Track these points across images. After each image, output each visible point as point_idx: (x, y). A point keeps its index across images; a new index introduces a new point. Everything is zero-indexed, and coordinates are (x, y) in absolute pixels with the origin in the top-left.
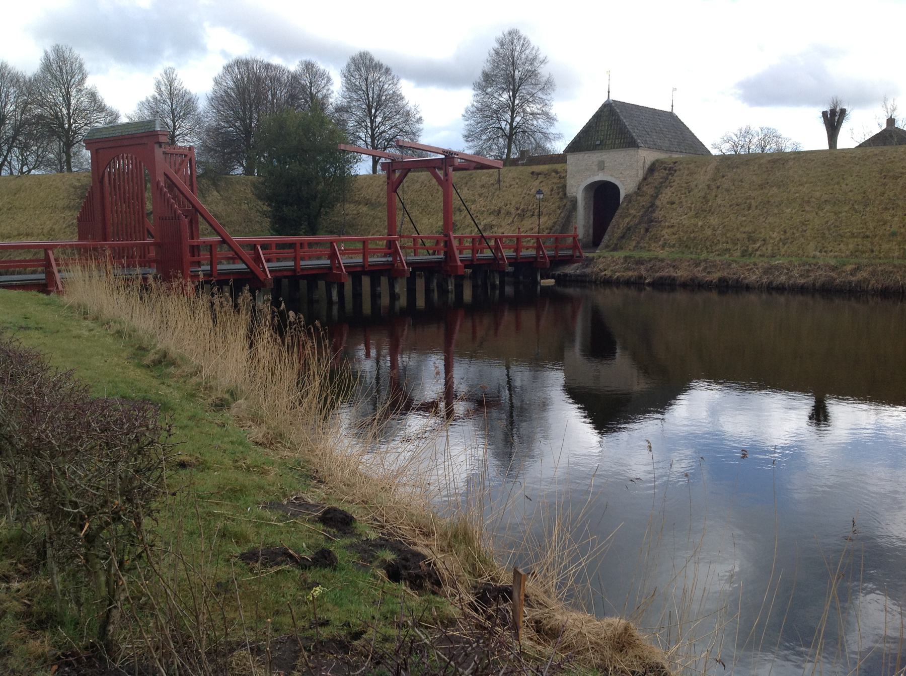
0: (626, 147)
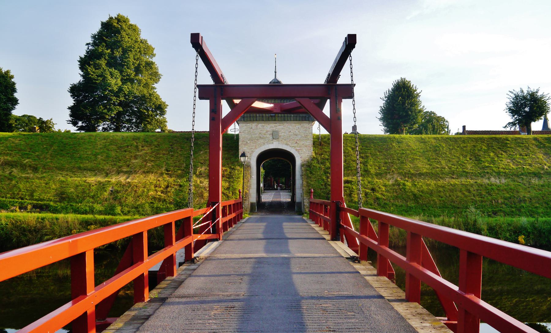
0: (299, 120)
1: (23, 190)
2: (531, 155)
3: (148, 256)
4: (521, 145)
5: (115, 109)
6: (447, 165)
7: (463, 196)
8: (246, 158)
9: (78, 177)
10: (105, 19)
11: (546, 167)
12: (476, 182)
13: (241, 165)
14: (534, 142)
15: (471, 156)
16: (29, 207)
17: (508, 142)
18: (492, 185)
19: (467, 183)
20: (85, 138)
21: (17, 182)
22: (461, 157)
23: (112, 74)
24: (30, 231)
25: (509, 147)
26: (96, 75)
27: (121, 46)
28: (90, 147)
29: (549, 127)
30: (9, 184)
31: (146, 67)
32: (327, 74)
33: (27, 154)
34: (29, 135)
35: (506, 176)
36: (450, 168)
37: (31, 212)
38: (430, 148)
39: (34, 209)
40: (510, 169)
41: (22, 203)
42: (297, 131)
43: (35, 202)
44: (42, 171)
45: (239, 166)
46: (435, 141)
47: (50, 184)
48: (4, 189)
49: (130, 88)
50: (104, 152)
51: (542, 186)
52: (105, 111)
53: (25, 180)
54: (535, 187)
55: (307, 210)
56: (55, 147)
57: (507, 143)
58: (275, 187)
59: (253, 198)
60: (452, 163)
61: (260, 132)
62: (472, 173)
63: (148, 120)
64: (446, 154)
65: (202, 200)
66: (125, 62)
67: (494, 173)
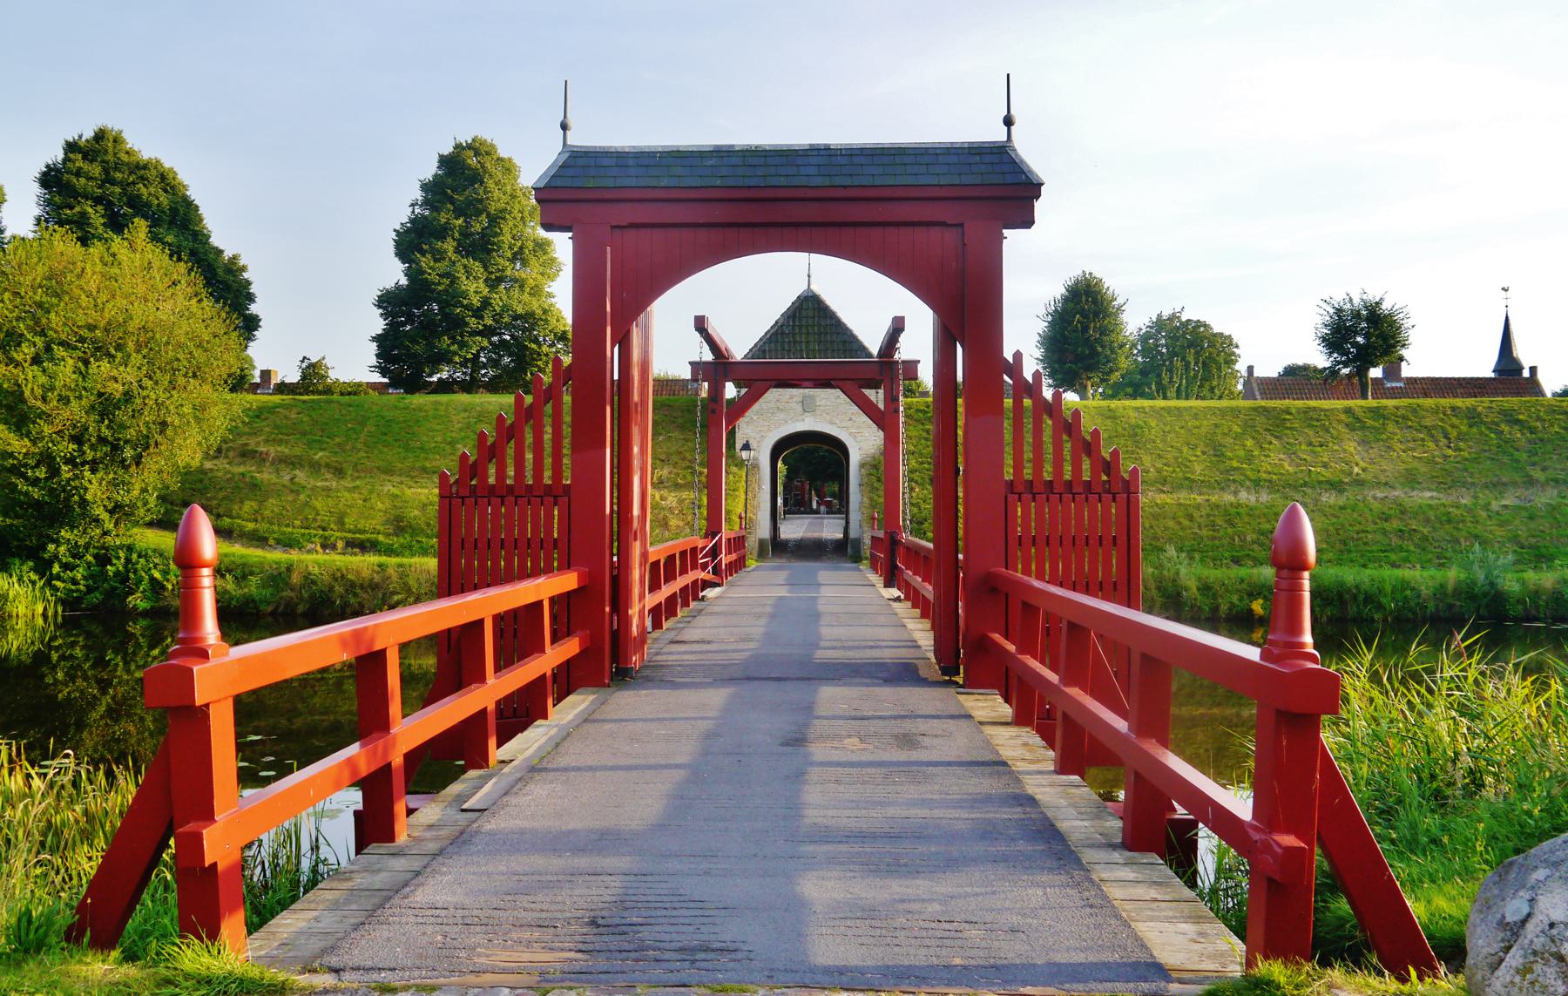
1: (323, 513)
2: (1330, 445)
3: (495, 672)
4: (1315, 423)
5: (474, 343)
6: (1154, 466)
7: (1177, 527)
8: (752, 452)
9: (423, 487)
10: (447, 150)
11: (1356, 470)
12: (1208, 500)
13: (741, 463)
14: (1343, 417)
15: (1206, 446)
16: (340, 544)
17: (1288, 417)
18: (1239, 505)
19: (1188, 502)
20: (426, 408)
21: (309, 496)
22: (1185, 449)
23: (468, 272)
24: (362, 586)
25: (1287, 428)
26: (437, 274)
27: (485, 209)
28: (438, 427)
29: (1515, 355)
30: (294, 501)
31: (534, 251)
33: (319, 441)
34: (313, 401)
35: (1272, 486)
36: (1159, 472)
37: (344, 554)
38: (1124, 429)
39: (350, 550)
40: (1282, 474)
41: (326, 538)
43: (350, 535)
44: (351, 475)
45: (736, 466)
46: (1136, 415)
47: (373, 501)
48: (288, 511)
49: (505, 298)
50: (467, 437)
51: (1342, 508)
52: (454, 348)
53: (324, 493)
54: (1327, 510)
55: (868, 555)
56: (370, 426)
57: (1285, 419)
58: (815, 506)
59: (763, 530)
60: (1165, 461)
62: (1202, 482)
63: (539, 363)
64: (1154, 442)
65: (667, 533)
66: (494, 244)
67: (1248, 483)
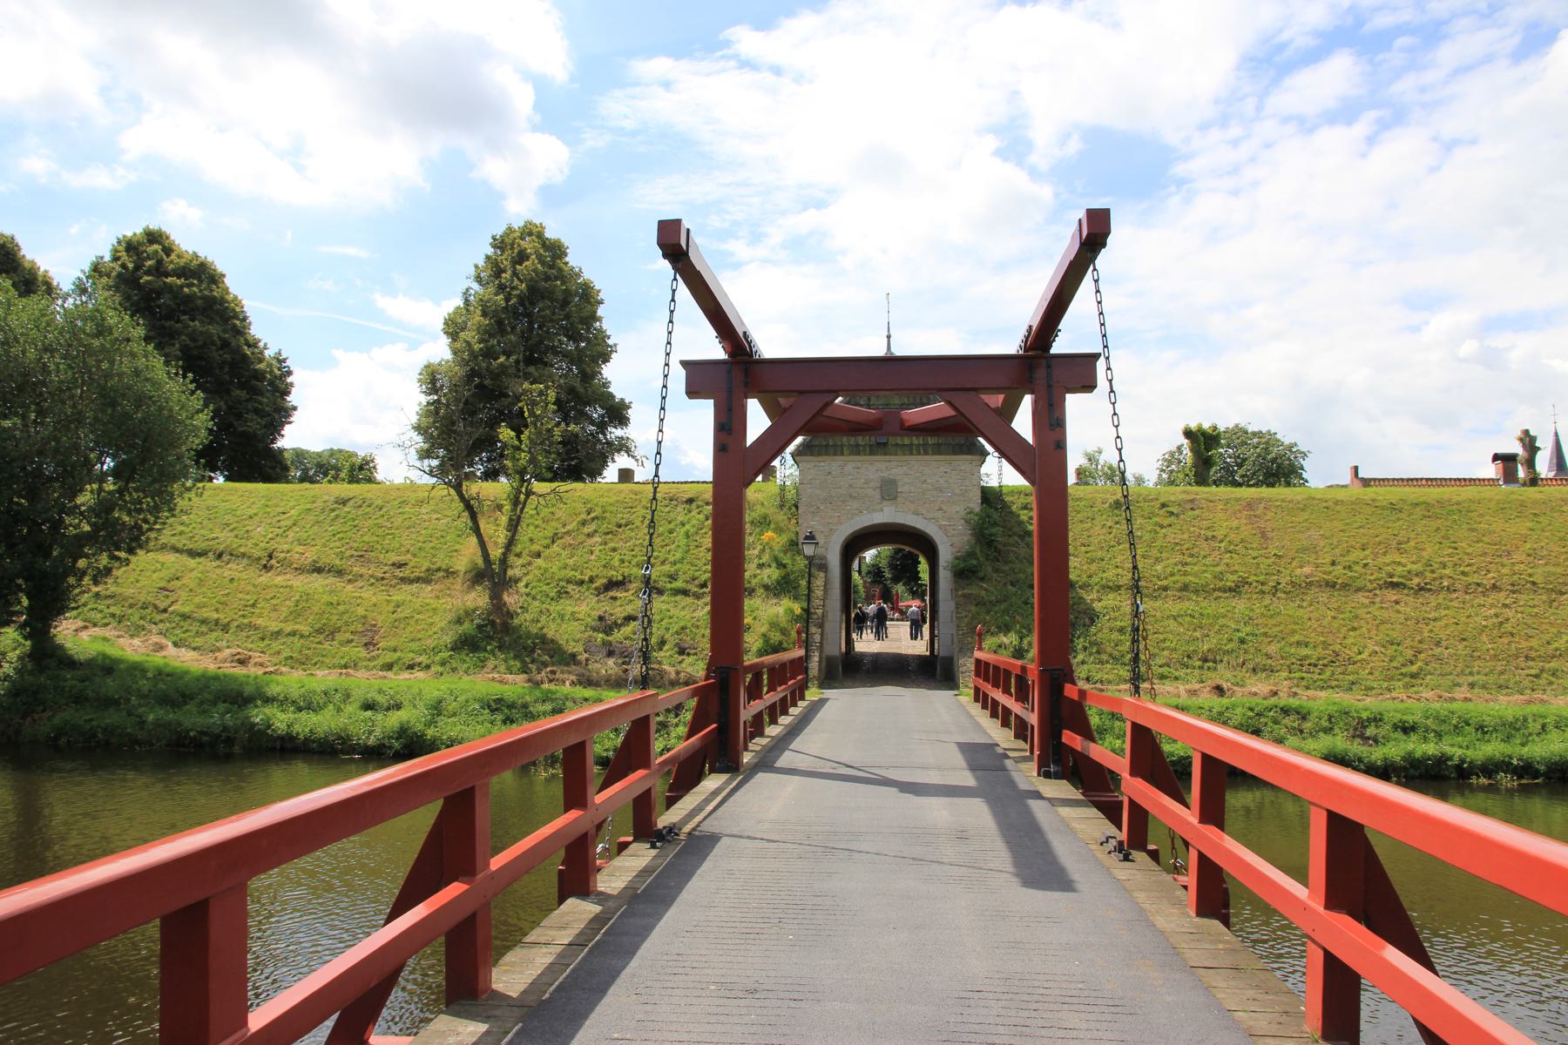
32: (1026, 327)
42: (942, 481)
61: (851, 482)
